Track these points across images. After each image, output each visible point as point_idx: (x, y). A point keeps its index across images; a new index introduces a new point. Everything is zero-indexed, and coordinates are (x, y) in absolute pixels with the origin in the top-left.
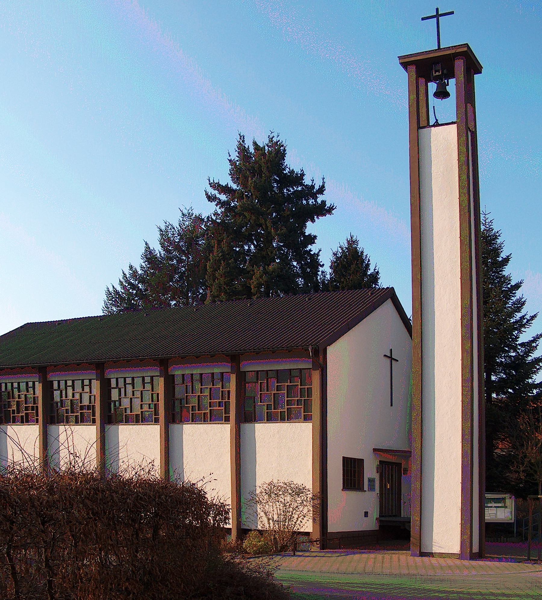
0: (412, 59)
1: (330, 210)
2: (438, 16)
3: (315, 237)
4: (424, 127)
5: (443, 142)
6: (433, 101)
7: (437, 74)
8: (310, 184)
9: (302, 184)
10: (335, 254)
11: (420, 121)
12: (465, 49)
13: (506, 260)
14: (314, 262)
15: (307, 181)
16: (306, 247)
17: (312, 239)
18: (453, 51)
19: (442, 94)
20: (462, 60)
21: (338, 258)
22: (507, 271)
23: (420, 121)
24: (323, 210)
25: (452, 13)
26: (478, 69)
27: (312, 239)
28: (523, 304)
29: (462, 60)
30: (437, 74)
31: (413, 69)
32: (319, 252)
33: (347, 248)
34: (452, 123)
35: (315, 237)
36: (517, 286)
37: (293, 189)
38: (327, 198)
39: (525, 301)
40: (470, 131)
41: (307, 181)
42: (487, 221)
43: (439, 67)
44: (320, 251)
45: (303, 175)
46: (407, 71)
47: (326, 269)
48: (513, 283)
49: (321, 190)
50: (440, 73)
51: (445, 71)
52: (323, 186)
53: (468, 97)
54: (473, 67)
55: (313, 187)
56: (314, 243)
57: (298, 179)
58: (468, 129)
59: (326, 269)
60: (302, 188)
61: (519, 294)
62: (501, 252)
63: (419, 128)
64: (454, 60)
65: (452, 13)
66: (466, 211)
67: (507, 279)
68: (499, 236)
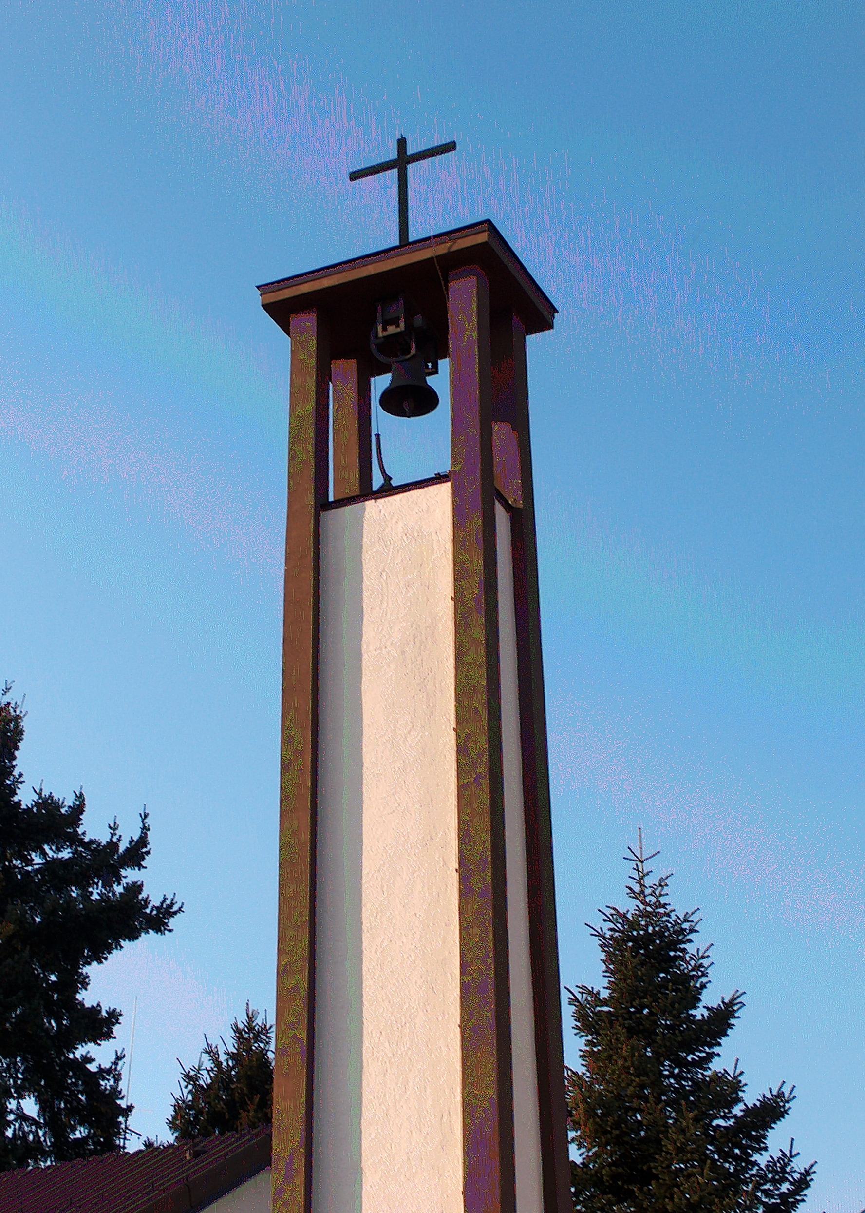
0: (306, 288)
1: (159, 920)
2: (403, 160)
3: (114, 1017)
4: (341, 503)
5: (406, 549)
6: (382, 421)
7: (392, 329)
8: (104, 838)
9: (75, 840)
10: (190, 1078)
11: (329, 483)
12: (482, 238)
13: (722, 1020)
14: (105, 1108)
15: (93, 828)
16: (72, 1048)
17: (100, 1025)
18: (442, 249)
19: (412, 400)
20: (475, 278)
21: (198, 1090)
22: (725, 1058)
23: (329, 483)
24: (136, 917)
25: (450, 147)
26: (538, 314)
27: (100, 1025)
28: (803, 1182)
29: (475, 278)
30: (392, 329)
31: (308, 322)
32: (116, 1064)
33: (232, 1056)
34: (439, 479)
35: (114, 1017)
36: (772, 1110)
37: (44, 854)
38: (153, 881)
39: (808, 1173)
40: (508, 507)
41: (93, 828)
42: (648, 881)
43: (398, 309)
44: (119, 1058)
45: (78, 810)
46: (289, 335)
47: (149, 1122)
48: (751, 1097)
49: (137, 853)
50: (402, 324)
51: (418, 321)
52: (143, 841)
53: (501, 401)
54: (518, 306)
55: (113, 846)
56: (108, 1035)
57: (56, 821)
58: (492, 494)
59: (149, 1122)
60: (75, 852)
61: (777, 1140)
62: (703, 986)
63: (323, 505)
64: (447, 283)
65: (450, 147)
66: (482, 769)
67: (728, 1089)
68: (692, 931)
